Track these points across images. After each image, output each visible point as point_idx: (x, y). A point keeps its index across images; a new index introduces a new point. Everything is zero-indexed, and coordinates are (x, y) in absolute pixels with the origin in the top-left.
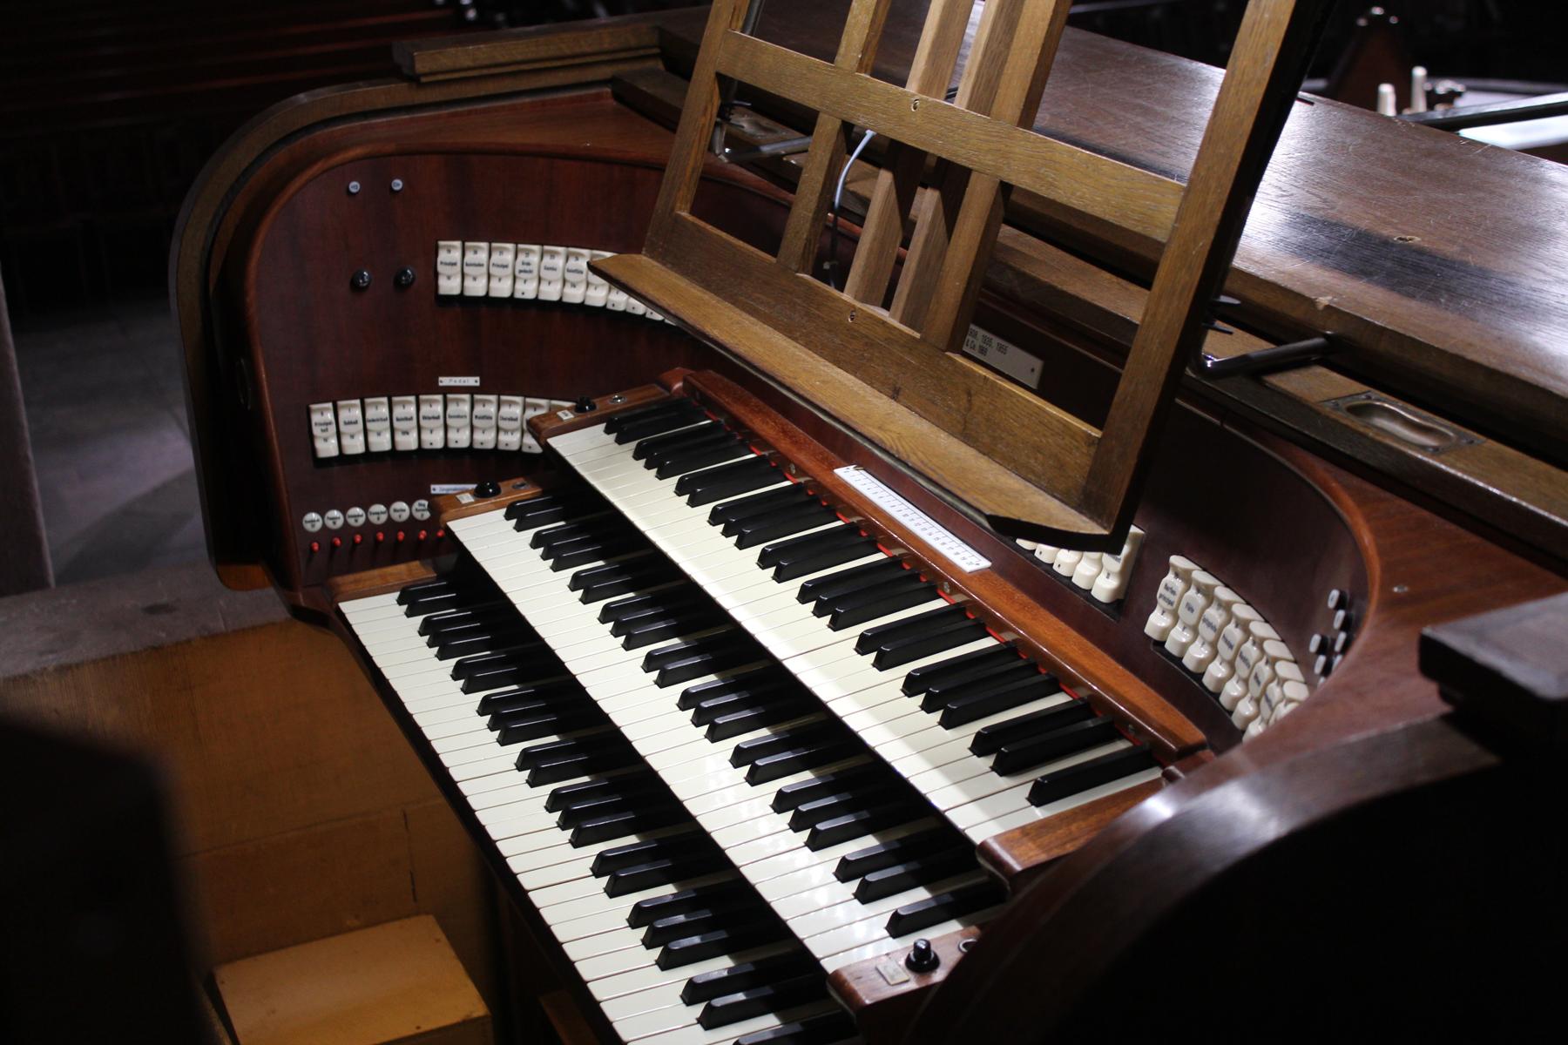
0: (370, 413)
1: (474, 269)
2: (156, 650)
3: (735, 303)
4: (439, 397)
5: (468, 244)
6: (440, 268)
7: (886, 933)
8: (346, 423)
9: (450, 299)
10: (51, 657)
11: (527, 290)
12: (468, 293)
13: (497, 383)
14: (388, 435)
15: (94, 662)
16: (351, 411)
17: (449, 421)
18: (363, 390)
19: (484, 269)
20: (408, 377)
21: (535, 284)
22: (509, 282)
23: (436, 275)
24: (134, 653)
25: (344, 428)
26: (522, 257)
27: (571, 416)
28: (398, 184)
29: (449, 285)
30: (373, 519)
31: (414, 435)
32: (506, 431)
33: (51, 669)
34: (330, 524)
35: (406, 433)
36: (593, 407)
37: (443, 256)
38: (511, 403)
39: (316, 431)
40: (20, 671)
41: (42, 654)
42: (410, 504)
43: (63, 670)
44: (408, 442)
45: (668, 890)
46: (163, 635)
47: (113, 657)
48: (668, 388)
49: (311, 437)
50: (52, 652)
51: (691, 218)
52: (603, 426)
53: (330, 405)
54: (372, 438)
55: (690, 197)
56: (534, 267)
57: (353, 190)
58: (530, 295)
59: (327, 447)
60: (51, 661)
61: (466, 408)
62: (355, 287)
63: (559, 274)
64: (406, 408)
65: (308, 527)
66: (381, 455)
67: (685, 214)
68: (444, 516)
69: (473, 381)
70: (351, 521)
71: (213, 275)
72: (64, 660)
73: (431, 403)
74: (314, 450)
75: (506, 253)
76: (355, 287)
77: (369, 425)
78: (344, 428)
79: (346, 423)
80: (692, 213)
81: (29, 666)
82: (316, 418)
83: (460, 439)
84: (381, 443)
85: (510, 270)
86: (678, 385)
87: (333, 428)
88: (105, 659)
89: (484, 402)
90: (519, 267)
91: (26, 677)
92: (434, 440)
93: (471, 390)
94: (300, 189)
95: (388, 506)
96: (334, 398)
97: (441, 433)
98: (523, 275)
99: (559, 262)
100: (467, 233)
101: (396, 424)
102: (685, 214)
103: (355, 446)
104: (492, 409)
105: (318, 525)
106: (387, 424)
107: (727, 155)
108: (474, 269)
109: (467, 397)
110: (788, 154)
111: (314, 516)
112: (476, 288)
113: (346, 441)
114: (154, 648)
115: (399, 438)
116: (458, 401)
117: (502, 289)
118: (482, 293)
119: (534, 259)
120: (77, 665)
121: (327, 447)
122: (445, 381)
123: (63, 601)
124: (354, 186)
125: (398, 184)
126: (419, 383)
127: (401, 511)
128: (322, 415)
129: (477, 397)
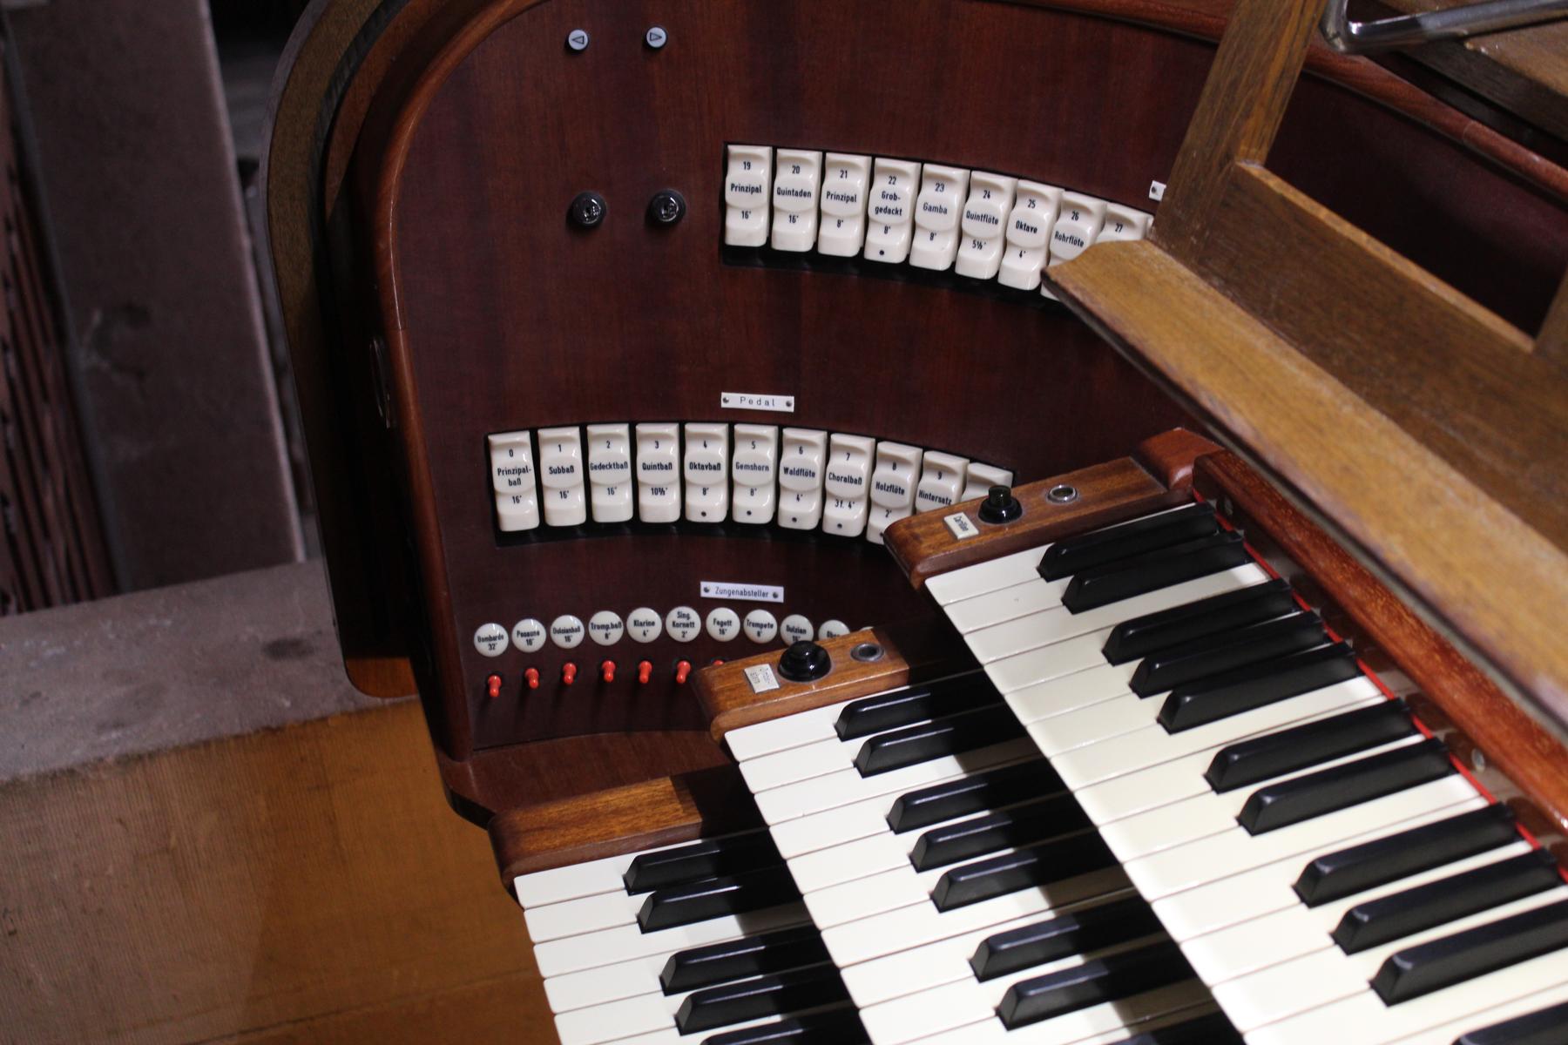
0: (597, 454)
1: (794, 201)
2: (273, 732)
3: (1401, 417)
4: (720, 430)
5: (783, 153)
6: (730, 196)
7: (1206, 786)
8: (553, 471)
9: (744, 254)
10: (114, 735)
11: (889, 246)
12: (780, 245)
13: (826, 411)
14: (627, 495)
15: (177, 750)
16: (562, 447)
17: (738, 475)
18: (582, 412)
19: (811, 203)
20: (667, 389)
21: (904, 235)
22: (856, 229)
23: (723, 207)
24: (237, 737)
25: (549, 479)
26: (881, 184)
27: (973, 531)
28: (658, 37)
29: (745, 229)
30: (598, 636)
31: (674, 495)
32: (839, 501)
33: (110, 759)
34: (521, 643)
35: (659, 491)
36: (1015, 512)
37: (736, 174)
38: (849, 451)
39: (500, 483)
40: (62, 763)
41: (102, 727)
42: (664, 614)
43: (129, 761)
44: (662, 508)
45: (985, 813)
46: (288, 704)
47: (207, 744)
48: (1163, 476)
49: (492, 494)
50: (118, 725)
51: (1274, 183)
52: (1038, 553)
53: (524, 437)
54: (599, 498)
55: (1270, 131)
56: (905, 204)
57: (576, 46)
58: (895, 256)
59: (518, 514)
60: (114, 743)
61: (767, 453)
62: (575, 223)
63: (950, 221)
64: (660, 441)
65: (483, 648)
66: (614, 528)
67: (1256, 169)
68: (722, 720)
69: (782, 403)
70: (559, 640)
71: (335, 182)
72: (132, 746)
73: (705, 440)
74: (495, 517)
75: (851, 173)
76: (575, 223)
77: (595, 475)
78: (549, 479)
79: (553, 471)
80: (1271, 165)
81: (78, 753)
82: (500, 460)
83: (755, 508)
84: (614, 507)
85: (858, 207)
86: (1183, 473)
87: (529, 479)
88: (193, 747)
89: (801, 446)
90: (876, 200)
91: (71, 772)
92: (709, 506)
93: (780, 421)
94: (484, 38)
95: (624, 616)
96: (532, 421)
97: (722, 496)
98: (884, 218)
99: (952, 197)
100: (782, 133)
101: (642, 475)
102: (1256, 169)
103: (567, 511)
104: (814, 459)
105: (501, 646)
106: (628, 472)
107: (1349, 38)
108: (794, 201)
109: (770, 431)
110: (1473, 35)
111: (493, 629)
112: (795, 237)
113: (552, 502)
114: (269, 730)
115: (646, 499)
116: (754, 440)
117: (841, 241)
118: (805, 246)
119: (906, 188)
120: (151, 755)
121: (518, 514)
122: (733, 400)
123: (152, 621)
124: (578, 39)
125: (658, 37)
126: (688, 403)
127: (646, 623)
128: (509, 453)
129: (789, 433)
